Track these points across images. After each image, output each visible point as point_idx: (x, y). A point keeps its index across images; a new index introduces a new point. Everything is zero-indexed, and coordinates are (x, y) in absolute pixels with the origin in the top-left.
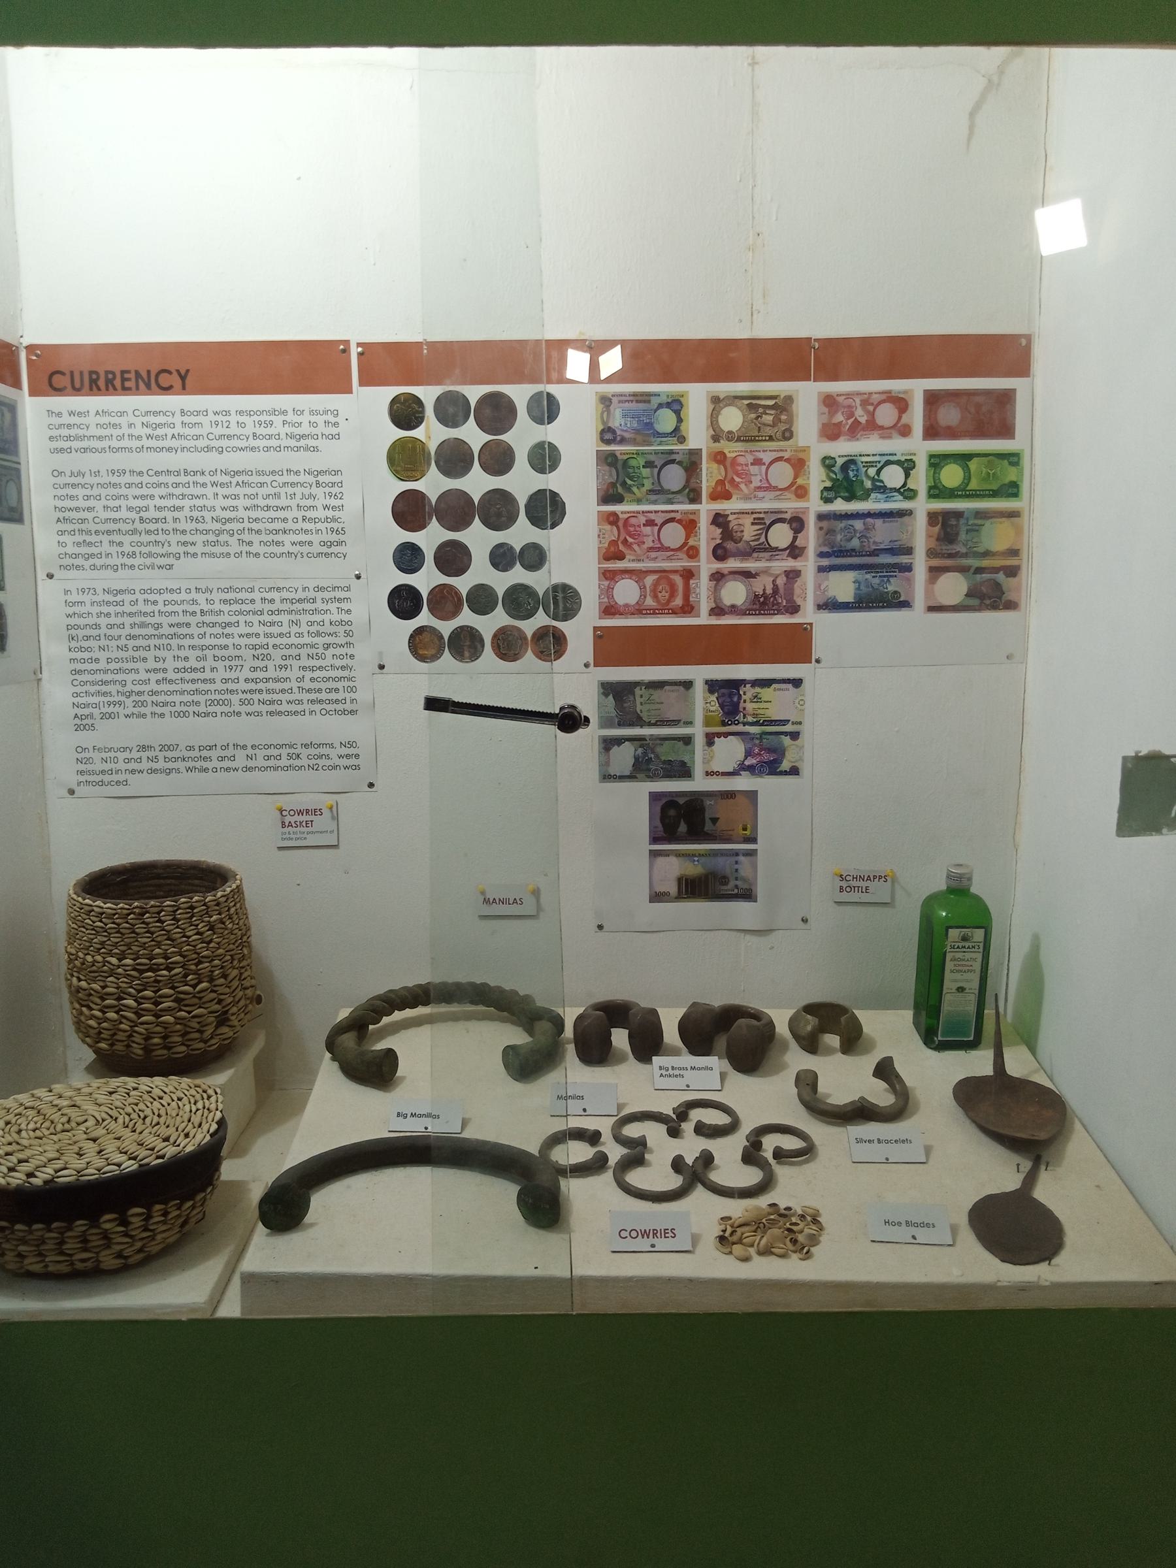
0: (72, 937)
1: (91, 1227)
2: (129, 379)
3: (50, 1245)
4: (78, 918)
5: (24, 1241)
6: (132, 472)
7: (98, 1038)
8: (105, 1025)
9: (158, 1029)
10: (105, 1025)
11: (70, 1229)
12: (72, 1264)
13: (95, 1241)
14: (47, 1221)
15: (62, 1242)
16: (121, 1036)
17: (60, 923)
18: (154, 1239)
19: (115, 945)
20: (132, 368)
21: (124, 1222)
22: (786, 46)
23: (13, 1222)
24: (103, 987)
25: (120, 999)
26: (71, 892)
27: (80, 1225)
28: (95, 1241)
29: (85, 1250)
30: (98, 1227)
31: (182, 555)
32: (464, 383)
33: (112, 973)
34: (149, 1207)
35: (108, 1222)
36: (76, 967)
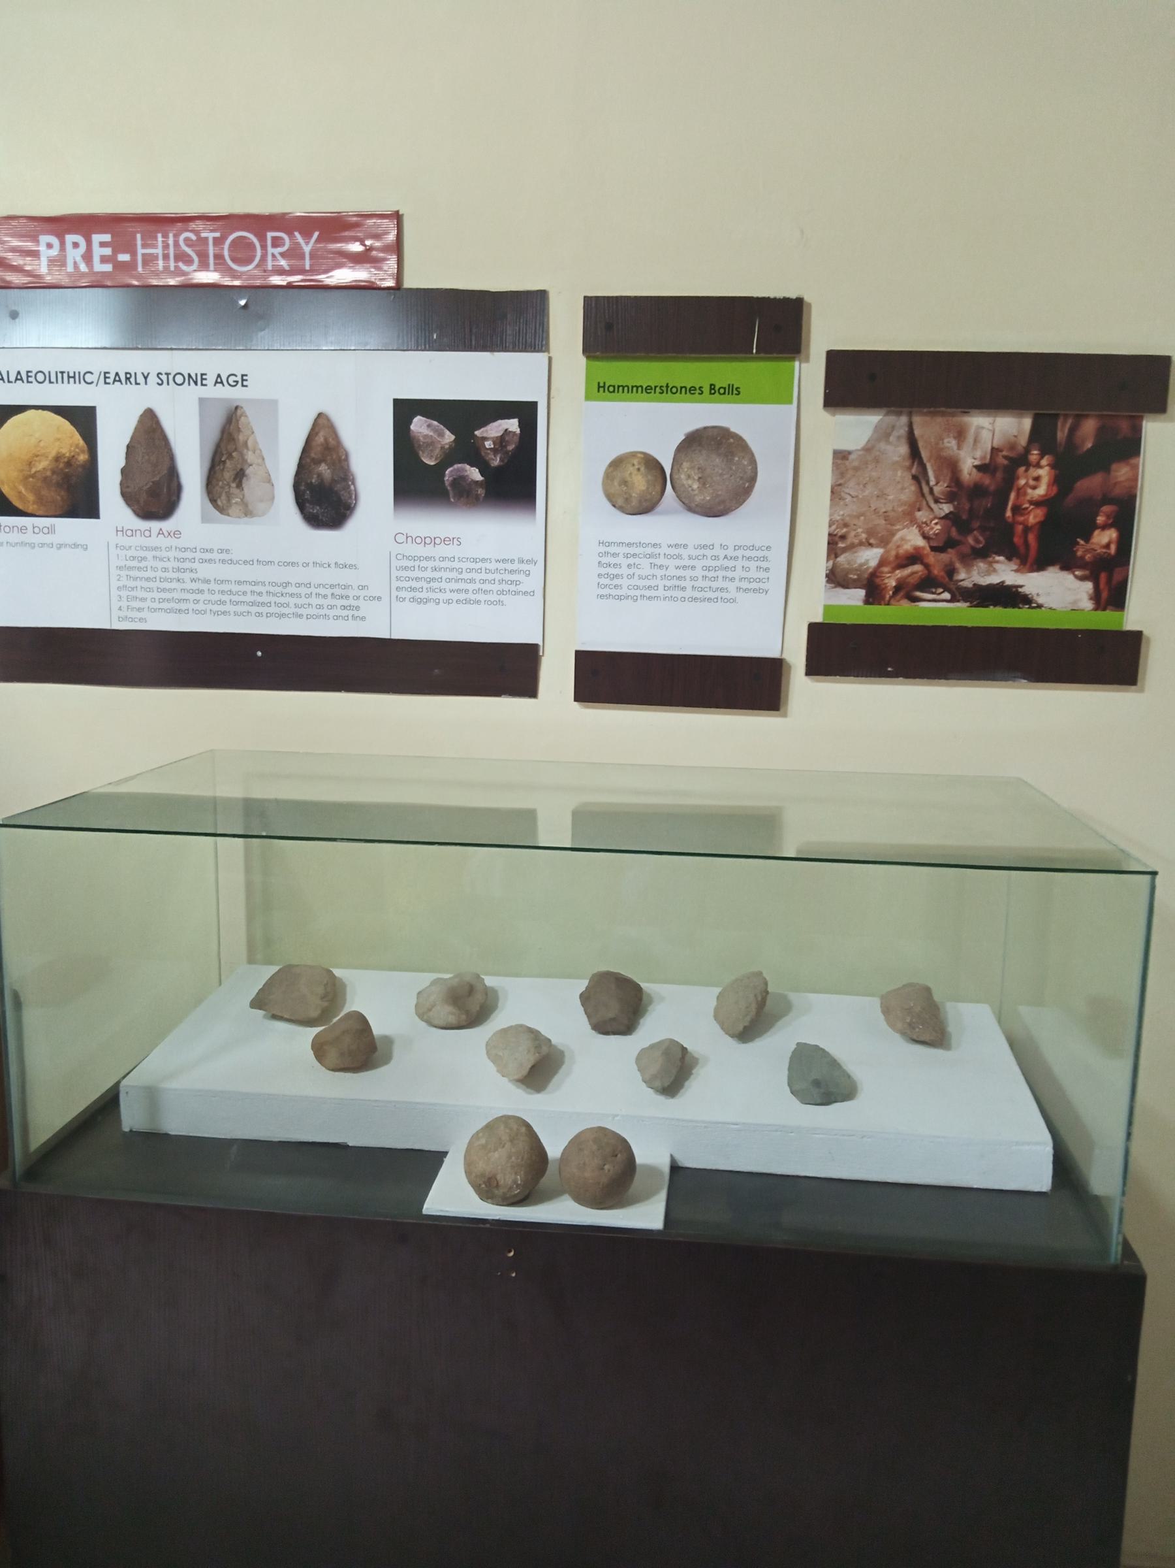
2: (31, 377)
20: (66, 370)
31: (639, 597)
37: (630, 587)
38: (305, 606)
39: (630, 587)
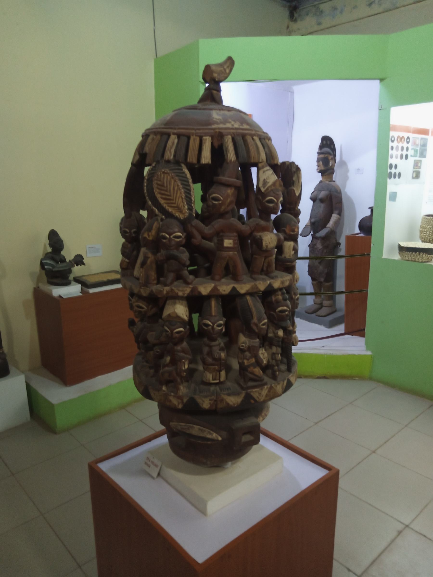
0: (421, 223)
1: (415, 254)
3: (410, 255)
4: (423, 218)
5: (406, 254)
7: (423, 238)
8: (424, 236)
9: (432, 238)
10: (424, 236)
11: (412, 253)
12: (412, 259)
13: (415, 256)
14: (410, 252)
15: (411, 255)
16: (426, 238)
17: (420, 220)
18: (423, 258)
19: (427, 224)
21: (420, 254)
22: (317, 161)
23: (405, 251)
24: (425, 230)
25: (427, 232)
27: (414, 253)
28: (415, 256)
29: (414, 257)
30: (416, 254)
32: (389, 137)
33: (426, 228)
34: (423, 253)
35: (417, 253)
36: (421, 227)
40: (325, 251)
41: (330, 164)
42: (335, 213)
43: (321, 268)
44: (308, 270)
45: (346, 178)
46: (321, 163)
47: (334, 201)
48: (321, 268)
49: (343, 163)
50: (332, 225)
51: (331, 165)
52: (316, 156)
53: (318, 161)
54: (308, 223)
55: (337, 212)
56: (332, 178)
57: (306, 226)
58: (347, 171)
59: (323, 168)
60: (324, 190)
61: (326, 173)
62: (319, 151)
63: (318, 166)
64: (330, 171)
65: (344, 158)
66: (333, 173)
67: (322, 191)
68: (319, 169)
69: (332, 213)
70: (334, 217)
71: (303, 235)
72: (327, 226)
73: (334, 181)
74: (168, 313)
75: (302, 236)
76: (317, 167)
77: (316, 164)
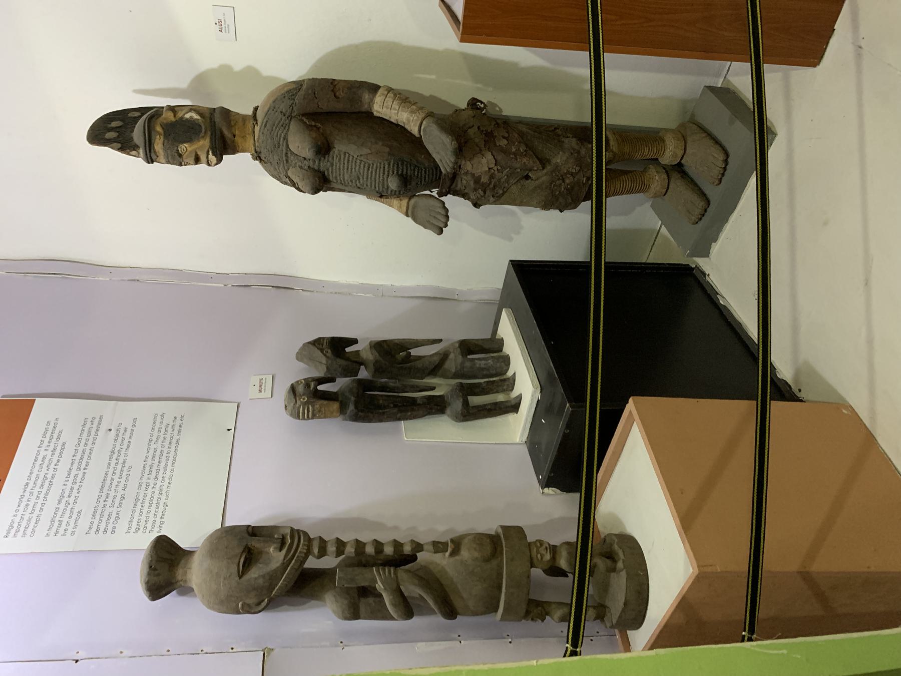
6: (58, 461)
26: (447, 554)
37: (144, 532)
38: (168, 494)
39: (144, 532)
40: (504, 142)
41: (191, 117)
42: (372, 101)
43: (559, 159)
44: (557, 212)
45: (251, 73)
46: (184, 147)
47: (326, 104)
48: (559, 159)
49: (201, 81)
50: (412, 112)
51: (196, 116)
52: (162, 171)
53: (177, 159)
54: (399, 209)
55: (366, 96)
56: (244, 118)
57: (410, 213)
58: (225, 70)
59: (204, 143)
60: (285, 139)
61: (226, 133)
62: (141, 151)
63: (197, 160)
64: (218, 118)
65: (184, 84)
66: (226, 113)
67: (287, 146)
68: (208, 154)
69: (369, 115)
70: (382, 107)
71: (441, 225)
72: (415, 131)
73: (256, 109)
74: (206, 141)
75: (446, 226)
76: (203, 166)
77: (191, 170)
